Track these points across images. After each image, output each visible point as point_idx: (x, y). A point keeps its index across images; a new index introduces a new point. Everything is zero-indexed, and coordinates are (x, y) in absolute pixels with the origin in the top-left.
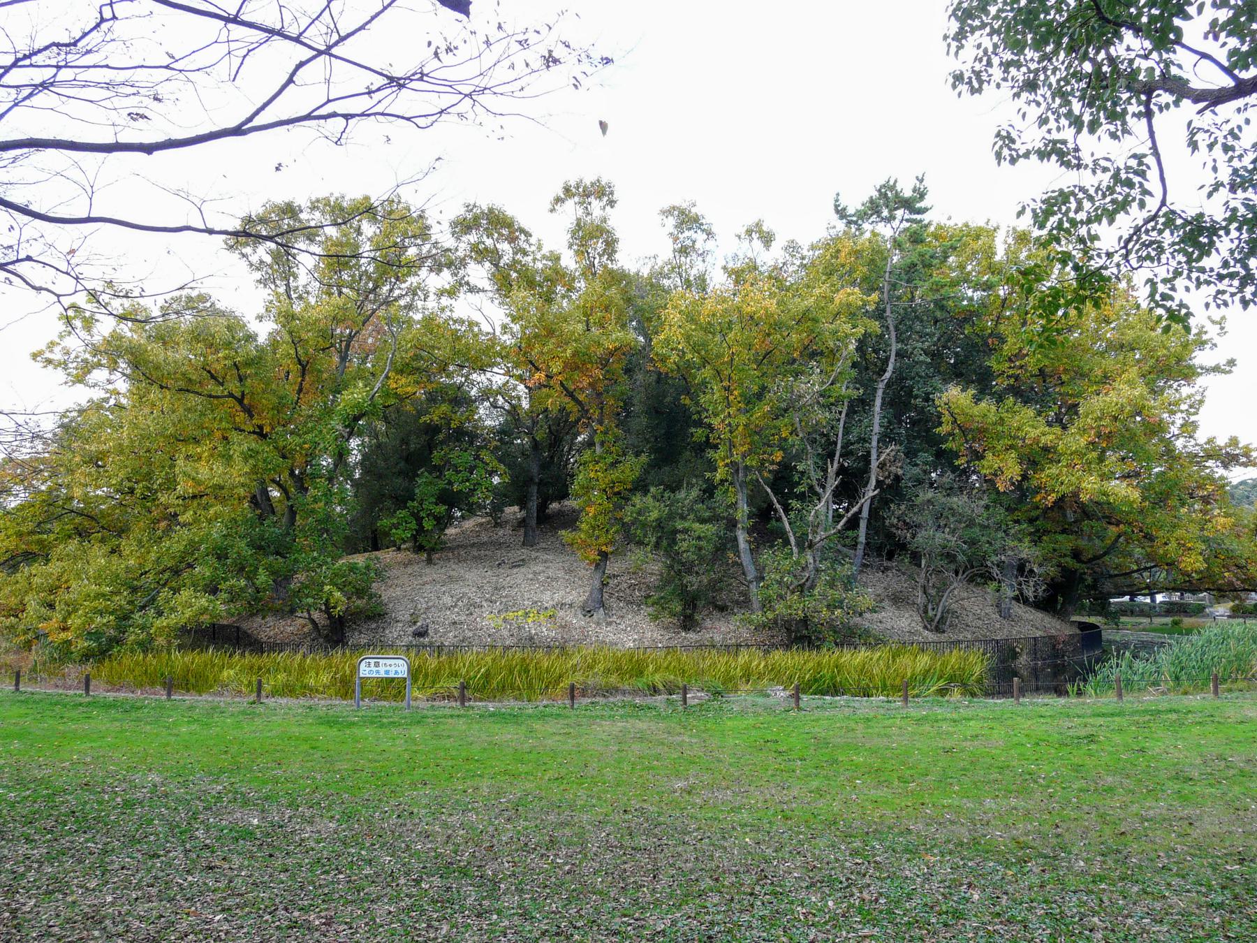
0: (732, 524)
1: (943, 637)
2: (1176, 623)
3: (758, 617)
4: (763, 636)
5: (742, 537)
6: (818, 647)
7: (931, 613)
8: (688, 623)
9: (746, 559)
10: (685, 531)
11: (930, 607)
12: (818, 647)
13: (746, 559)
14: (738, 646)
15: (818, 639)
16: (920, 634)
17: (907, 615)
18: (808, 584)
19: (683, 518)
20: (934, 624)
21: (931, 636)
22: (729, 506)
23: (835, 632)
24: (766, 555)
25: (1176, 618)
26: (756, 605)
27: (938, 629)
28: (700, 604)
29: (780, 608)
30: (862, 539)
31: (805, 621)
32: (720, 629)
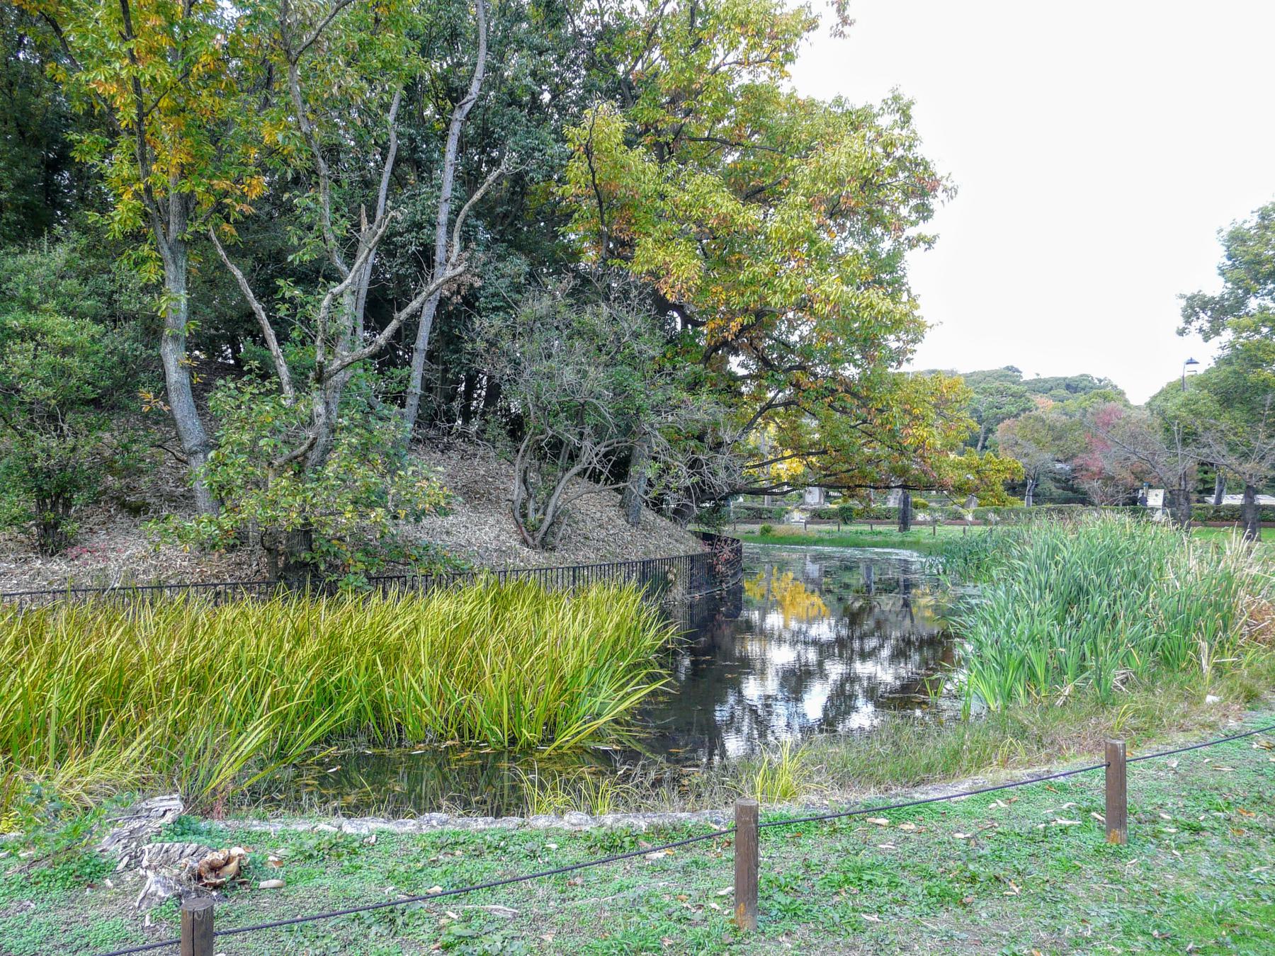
0: (152, 330)
1: (554, 559)
2: (766, 531)
3: (203, 524)
4: (215, 564)
5: (174, 359)
6: (332, 590)
7: (532, 517)
8: (52, 541)
9: (181, 405)
10: (28, 334)
11: (531, 506)
12: (332, 590)
13: (181, 405)
14: (160, 587)
15: (332, 568)
16: (517, 555)
17: (491, 521)
18: (314, 456)
19: (29, 307)
20: (539, 536)
21: (536, 558)
22: (146, 289)
23: (367, 554)
24: (223, 395)
25: (766, 525)
26: (203, 501)
27: (545, 546)
28: (79, 499)
29: (250, 506)
30: (416, 386)
31: (306, 533)
32: (123, 552)
